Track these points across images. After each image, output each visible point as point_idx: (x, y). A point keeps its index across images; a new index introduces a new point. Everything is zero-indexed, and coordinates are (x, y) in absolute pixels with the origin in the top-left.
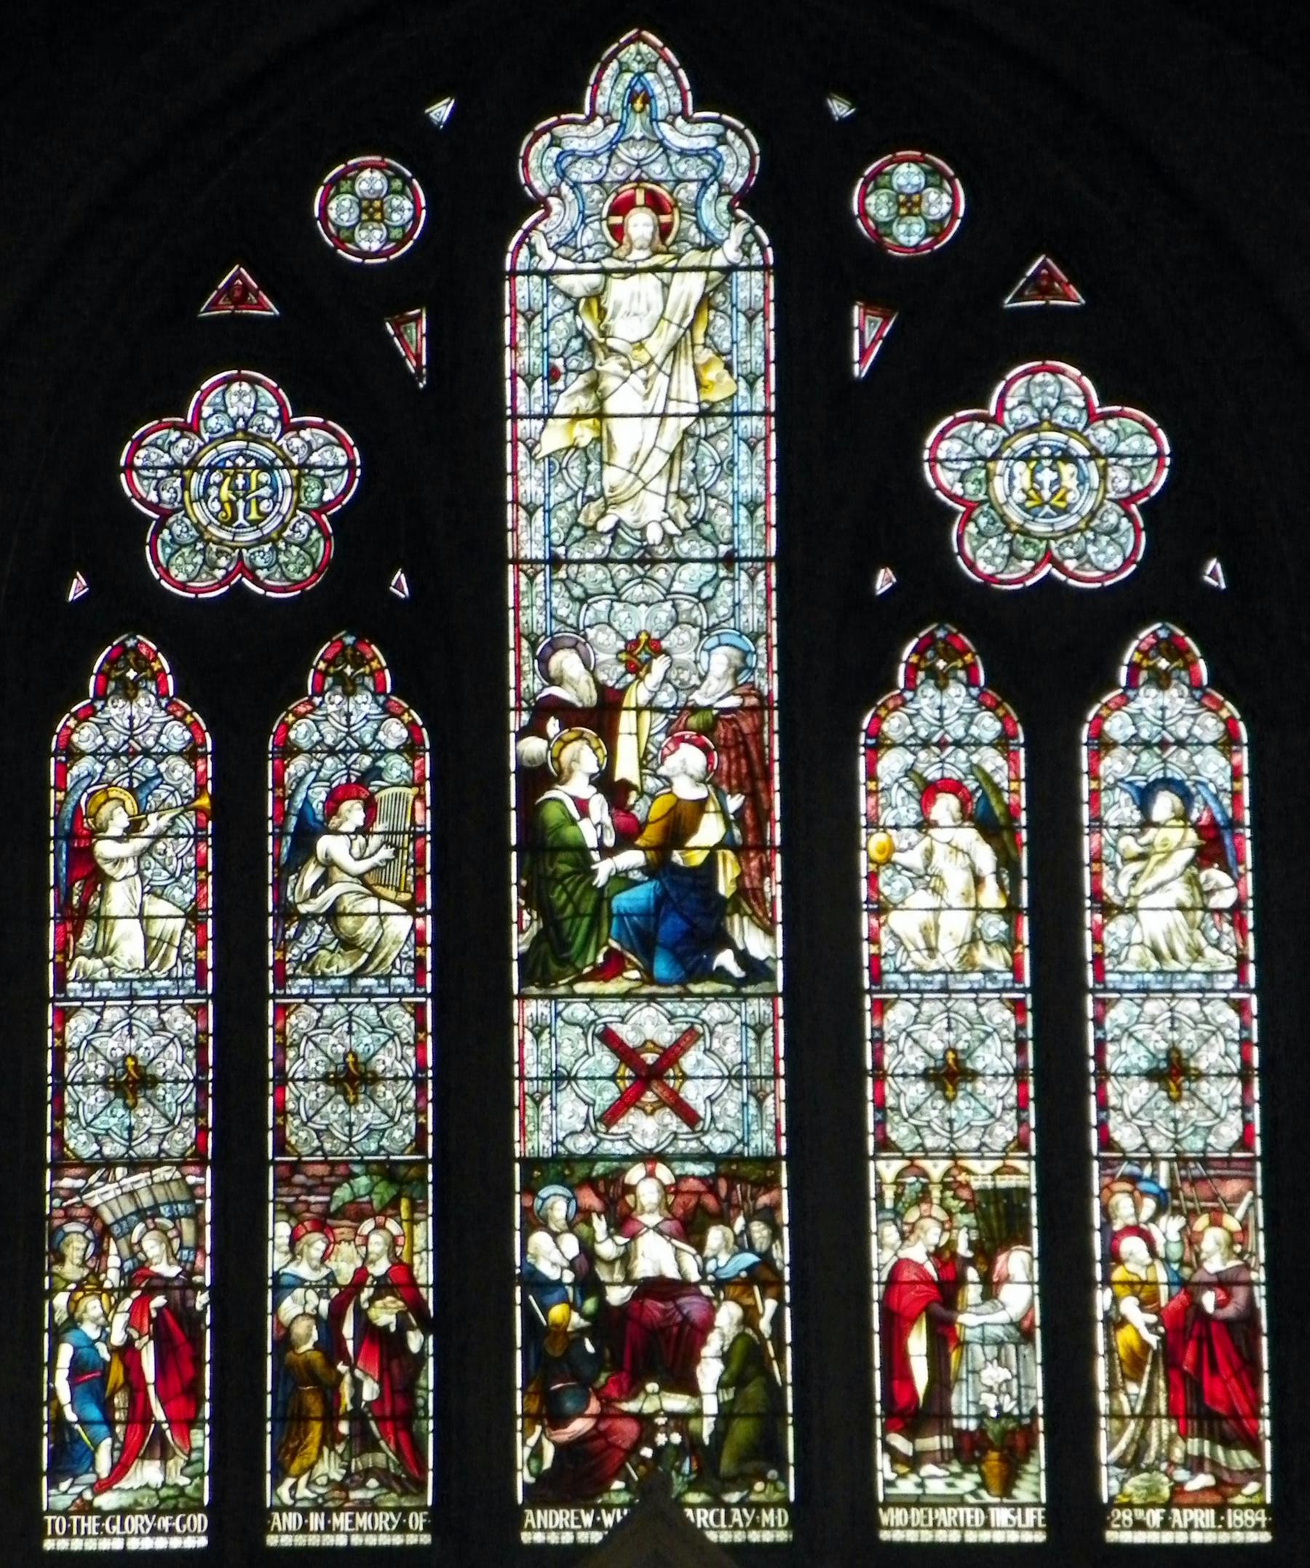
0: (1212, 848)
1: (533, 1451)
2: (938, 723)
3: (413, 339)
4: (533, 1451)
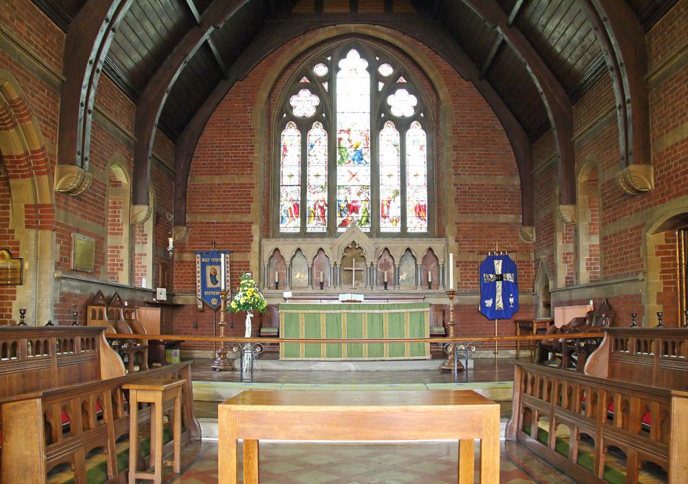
0: (421, 148)
1: (339, 221)
2: (389, 133)
3: (326, 86)
4: (339, 221)
